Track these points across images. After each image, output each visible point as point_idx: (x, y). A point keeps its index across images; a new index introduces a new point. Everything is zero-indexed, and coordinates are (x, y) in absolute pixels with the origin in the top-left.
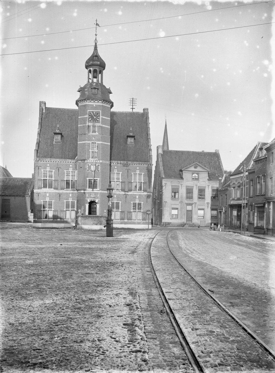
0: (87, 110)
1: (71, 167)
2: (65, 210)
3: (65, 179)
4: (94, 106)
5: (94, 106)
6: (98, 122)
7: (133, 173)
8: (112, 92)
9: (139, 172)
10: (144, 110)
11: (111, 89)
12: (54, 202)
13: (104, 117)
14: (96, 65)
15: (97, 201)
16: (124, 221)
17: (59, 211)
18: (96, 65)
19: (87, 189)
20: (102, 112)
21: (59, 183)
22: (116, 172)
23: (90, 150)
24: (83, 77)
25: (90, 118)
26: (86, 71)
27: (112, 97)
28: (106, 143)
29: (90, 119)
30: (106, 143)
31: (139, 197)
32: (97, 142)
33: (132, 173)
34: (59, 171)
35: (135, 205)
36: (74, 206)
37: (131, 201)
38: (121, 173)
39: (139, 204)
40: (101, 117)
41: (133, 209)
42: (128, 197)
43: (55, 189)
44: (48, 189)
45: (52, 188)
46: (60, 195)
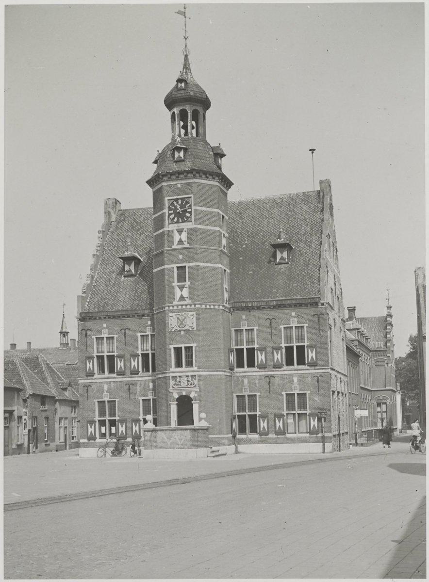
0: (164, 197)
1: (105, 328)
2: (285, 413)
3: (95, 354)
4: (179, 186)
5: (179, 186)
6: (188, 220)
7: (282, 327)
8: (225, 153)
9: (109, 334)
10: (321, 182)
11: (222, 147)
12: (118, 401)
13: (198, 208)
14: (188, 104)
15: (192, 396)
16: (267, 437)
17: (129, 420)
18: (188, 104)
19: (171, 370)
20: (169, 196)
21: (127, 362)
22: (244, 328)
23: (173, 284)
24: (162, 130)
25: (171, 214)
26: (168, 114)
27: (227, 167)
28: (209, 265)
29: (172, 216)
30: (209, 265)
31: (299, 381)
32: (187, 265)
33: (281, 326)
34: (125, 337)
35: (290, 396)
36: (110, 408)
37: (282, 391)
38: (306, 325)
39: (302, 396)
40: (193, 207)
41: (288, 408)
42: (277, 381)
43: (310, 365)
44: (246, 368)
45: (254, 366)
46: (270, 378)
